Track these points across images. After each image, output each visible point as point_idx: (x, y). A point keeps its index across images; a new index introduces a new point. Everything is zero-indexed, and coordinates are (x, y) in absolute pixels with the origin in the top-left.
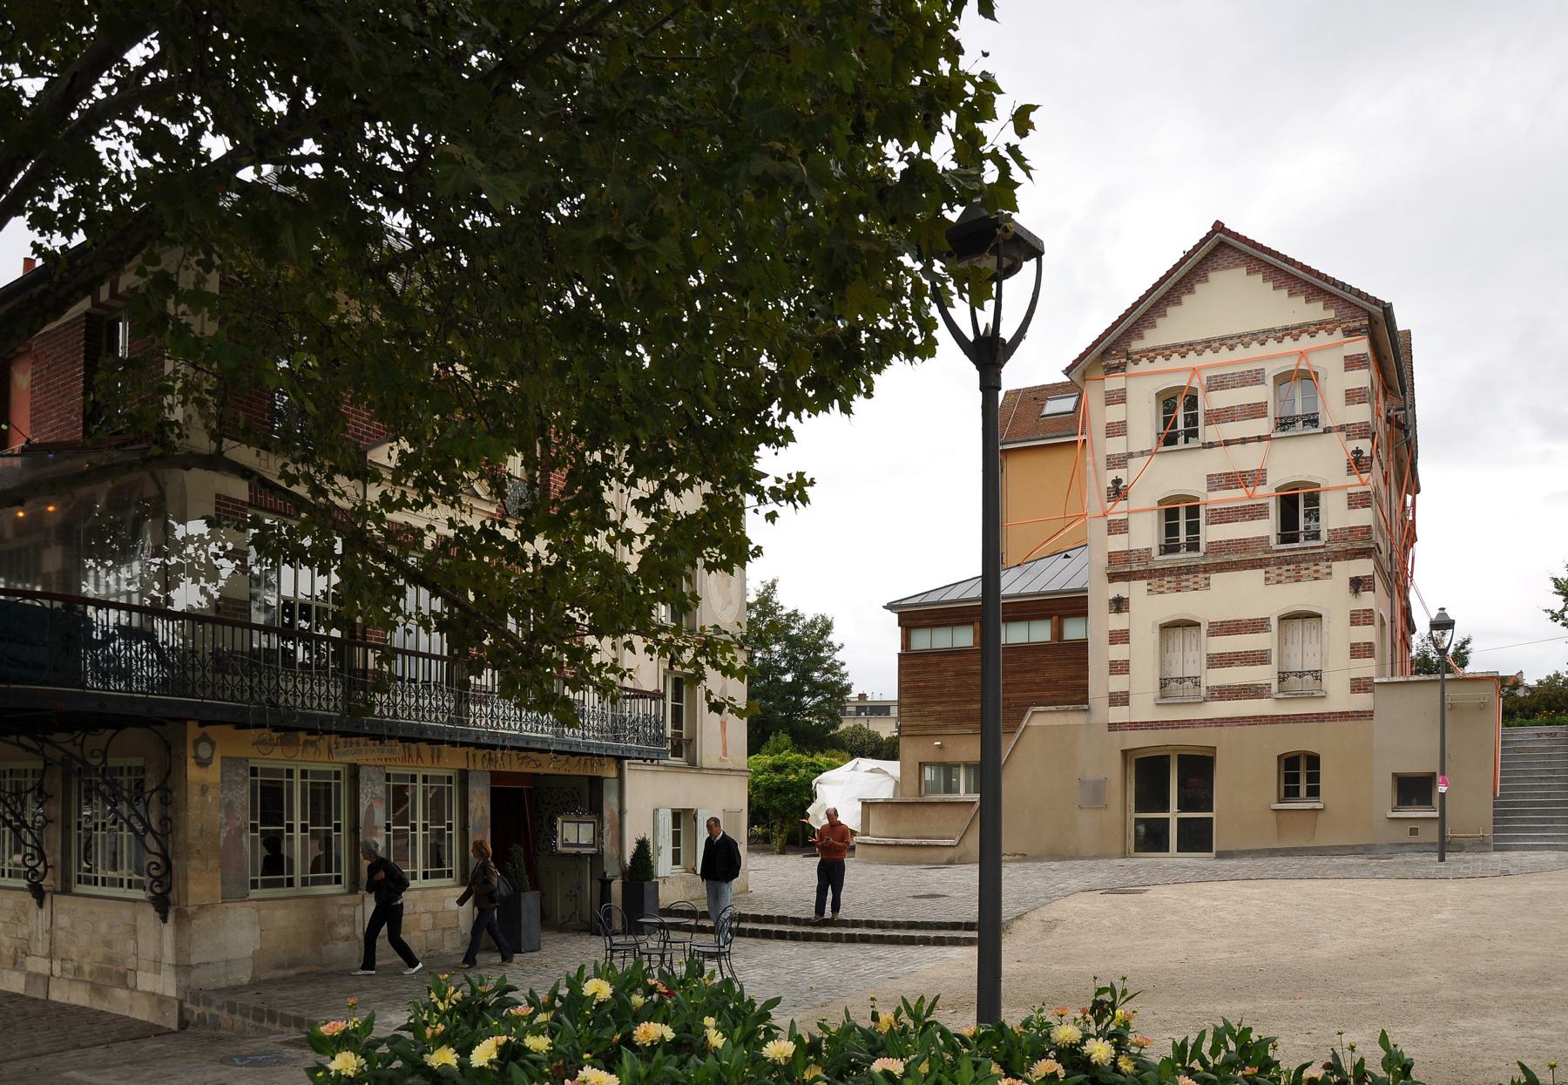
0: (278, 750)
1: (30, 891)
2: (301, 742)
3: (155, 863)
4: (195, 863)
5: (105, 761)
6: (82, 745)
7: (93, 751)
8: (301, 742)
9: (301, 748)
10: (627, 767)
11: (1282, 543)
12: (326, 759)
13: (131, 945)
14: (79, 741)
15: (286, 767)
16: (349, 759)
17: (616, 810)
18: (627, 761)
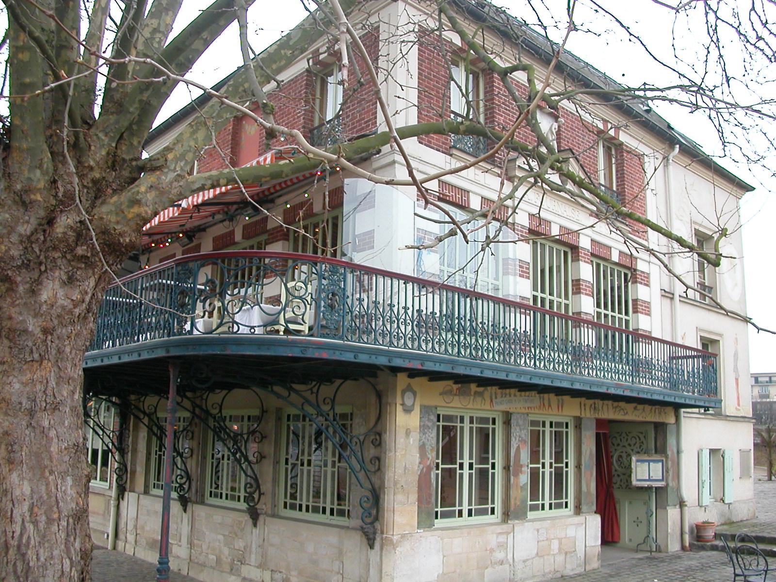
0: (456, 398)
1: (179, 501)
2: (472, 393)
3: (365, 496)
4: (400, 497)
5: (220, 411)
6: (144, 402)
7: (324, 399)
8: (472, 393)
9: (472, 398)
10: (682, 414)
11: (632, 300)
12: (489, 408)
13: (336, 566)
14: (205, 397)
15: (459, 415)
16: (504, 407)
17: (675, 451)
18: (683, 410)
